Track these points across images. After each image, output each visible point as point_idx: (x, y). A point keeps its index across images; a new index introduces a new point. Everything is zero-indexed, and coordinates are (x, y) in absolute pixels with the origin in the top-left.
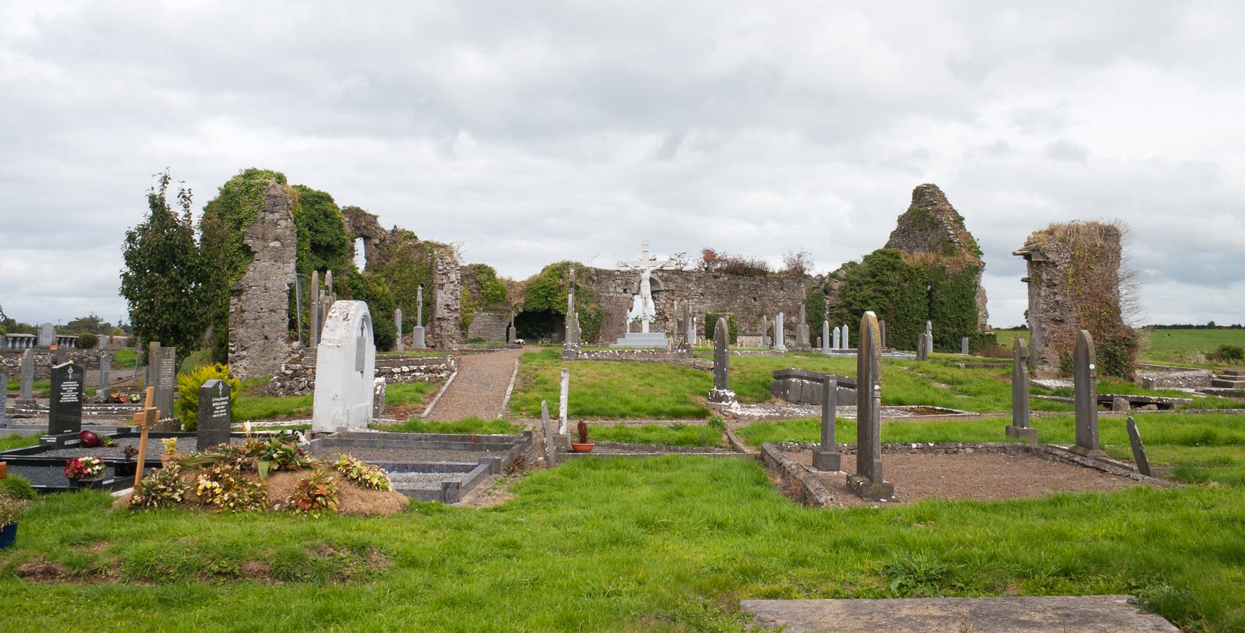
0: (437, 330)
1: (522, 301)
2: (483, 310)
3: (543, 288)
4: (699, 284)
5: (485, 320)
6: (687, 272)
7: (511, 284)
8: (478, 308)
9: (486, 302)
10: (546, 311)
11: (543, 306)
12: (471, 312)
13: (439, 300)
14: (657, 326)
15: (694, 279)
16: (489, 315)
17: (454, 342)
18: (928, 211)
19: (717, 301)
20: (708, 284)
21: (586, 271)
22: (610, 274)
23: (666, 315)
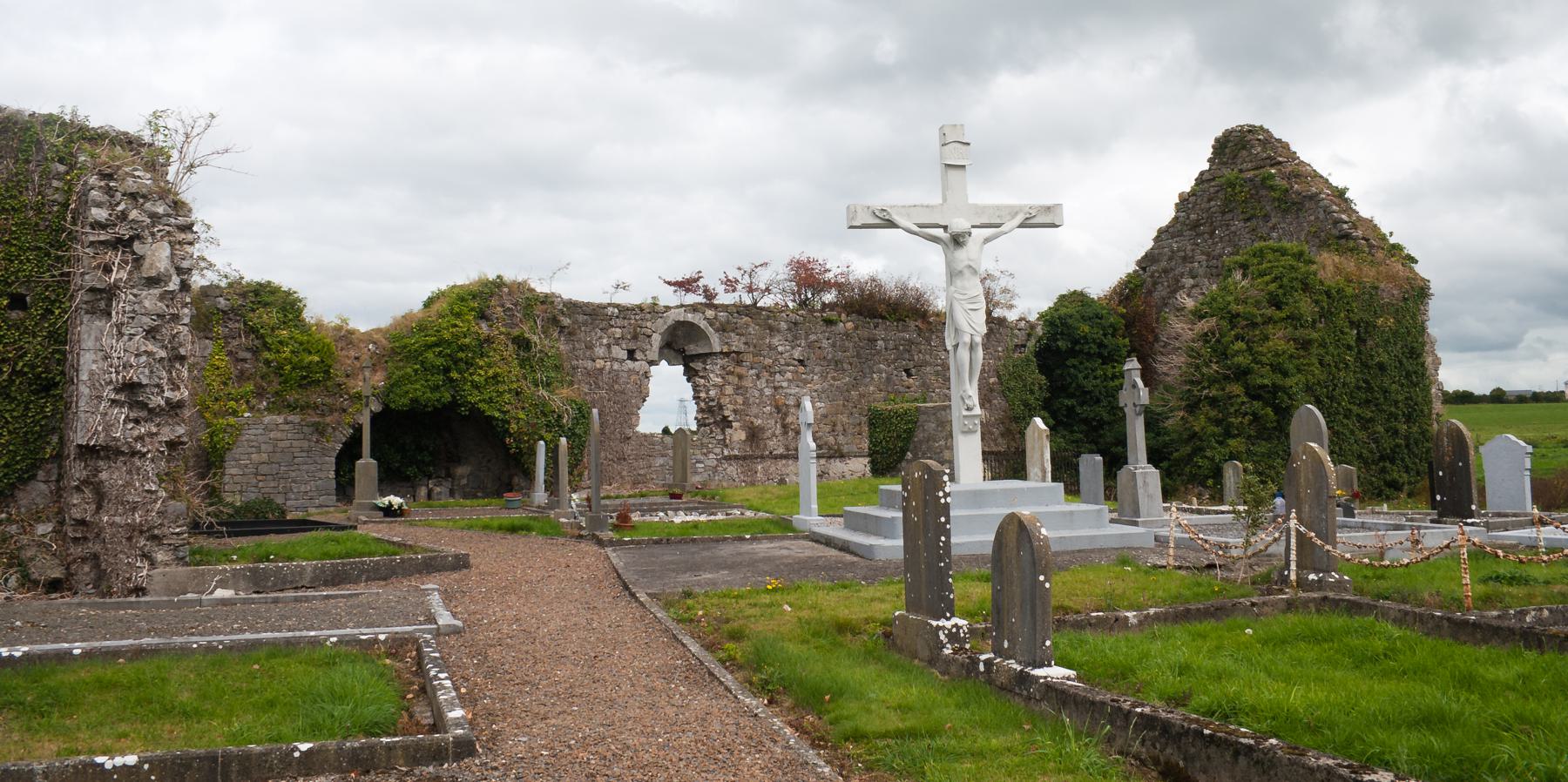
0: (79, 505)
1: (379, 380)
2: (267, 409)
3: (436, 345)
4: (796, 338)
5: (272, 435)
6: (767, 309)
7: (346, 337)
8: (253, 401)
9: (276, 387)
10: (444, 405)
11: (437, 395)
12: (234, 413)
13: (88, 363)
14: (705, 440)
15: (783, 325)
16: (287, 423)
17: (160, 556)
18: (1272, 176)
19: (834, 379)
20: (813, 337)
21: (543, 303)
22: (593, 314)
23: (726, 413)
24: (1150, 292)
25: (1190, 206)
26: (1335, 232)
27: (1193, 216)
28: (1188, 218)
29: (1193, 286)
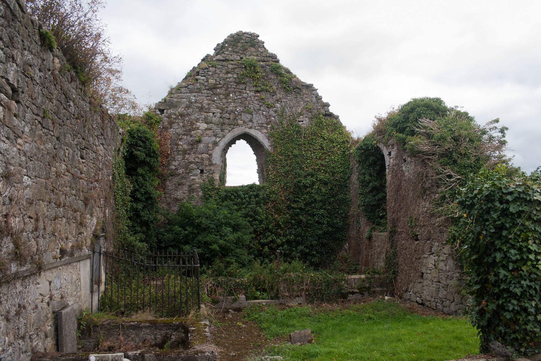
24: (165, 129)
25: (210, 73)
26: (323, 111)
27: (211, 81)
28: (207, 81)
29: (206, 129)
